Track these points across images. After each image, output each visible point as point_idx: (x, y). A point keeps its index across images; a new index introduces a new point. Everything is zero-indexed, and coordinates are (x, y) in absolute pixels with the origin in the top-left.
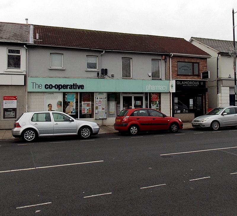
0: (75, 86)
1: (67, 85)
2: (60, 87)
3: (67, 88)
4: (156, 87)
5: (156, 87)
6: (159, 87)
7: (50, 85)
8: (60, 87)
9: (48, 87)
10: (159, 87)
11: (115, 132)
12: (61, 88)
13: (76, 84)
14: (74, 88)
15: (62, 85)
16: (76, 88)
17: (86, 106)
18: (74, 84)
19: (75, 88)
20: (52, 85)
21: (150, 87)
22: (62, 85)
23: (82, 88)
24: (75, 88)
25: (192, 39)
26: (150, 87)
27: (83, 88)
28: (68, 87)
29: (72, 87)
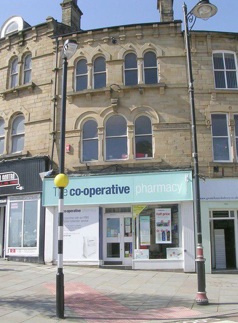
0: (115, 189)
1: (103, 189)
2: (92, 193)
3: (103, 193)
4: (156, 187)
5: (156, 187)
6: (163, 186)
7: (77, 190)
8: (92, 193)
9: (75, 192)
10: (163, 186)
11: (57, 155)
12: (94, 194)
13: (117, 185)
14: (113, 193)
15: (95, 189)
16: (117, 193)
17: (39, 80)
18: (113, 186)
19: (115, 192)
20: (79, 189)
21: (144, 188)
22: (95, 189)
23: (127, 191)
24: (115, 192)
25: (82, 160)
26: (144, 188)
27: (129, 192)
28: (105, 191)
29: (110, 190)
